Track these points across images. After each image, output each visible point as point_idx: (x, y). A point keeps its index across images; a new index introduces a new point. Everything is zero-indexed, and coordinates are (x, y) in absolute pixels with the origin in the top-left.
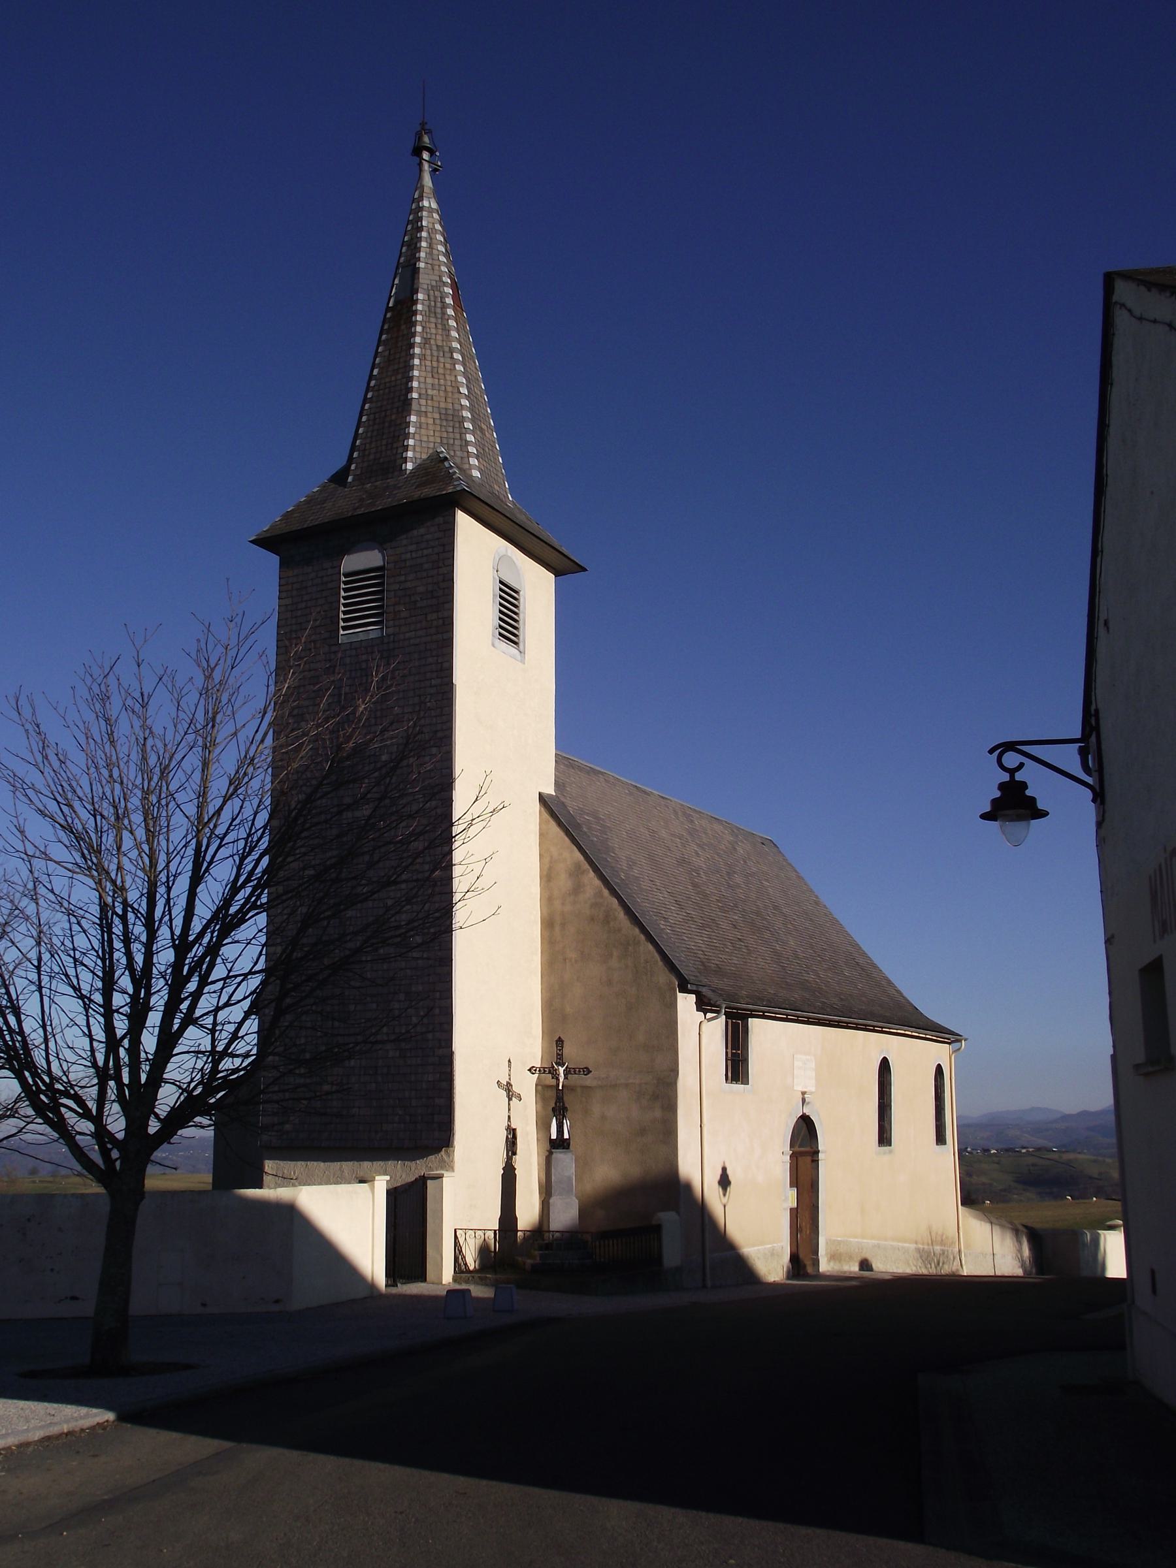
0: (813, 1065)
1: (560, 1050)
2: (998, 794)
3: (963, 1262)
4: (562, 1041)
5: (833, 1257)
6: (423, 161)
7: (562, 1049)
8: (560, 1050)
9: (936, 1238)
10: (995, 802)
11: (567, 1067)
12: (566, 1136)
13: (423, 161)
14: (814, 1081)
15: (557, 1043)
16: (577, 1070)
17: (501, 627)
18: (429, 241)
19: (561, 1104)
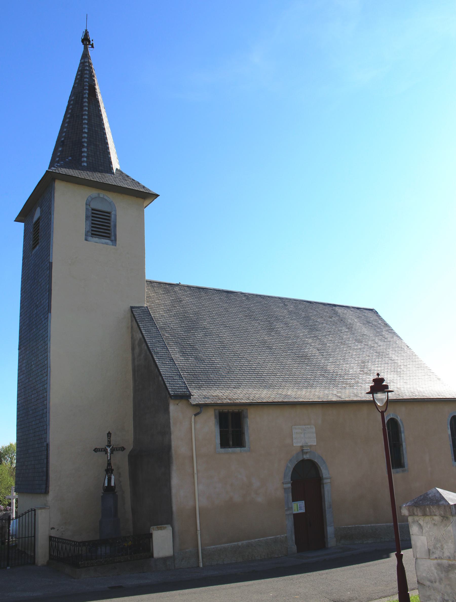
0: (314, 430)
1: (109, 438)
2: (372, 384)
3: (148, 351)
4: (111, 434)
5: (303, 502)
6: (393, 556)
7: (110, 438)
8: (109, 438)
9: (417, 510)
10: (371, 387)
11: (113, 447)
12: (113, 484)
13: (393, 556)
14: (315, 435)
15: (107, 435)
16: (118, 448)
17: (92, 223)
18: (90, 75)
19: (110, 467)
